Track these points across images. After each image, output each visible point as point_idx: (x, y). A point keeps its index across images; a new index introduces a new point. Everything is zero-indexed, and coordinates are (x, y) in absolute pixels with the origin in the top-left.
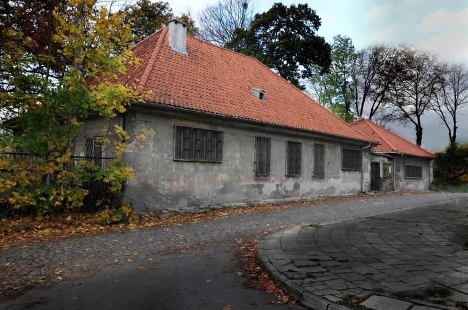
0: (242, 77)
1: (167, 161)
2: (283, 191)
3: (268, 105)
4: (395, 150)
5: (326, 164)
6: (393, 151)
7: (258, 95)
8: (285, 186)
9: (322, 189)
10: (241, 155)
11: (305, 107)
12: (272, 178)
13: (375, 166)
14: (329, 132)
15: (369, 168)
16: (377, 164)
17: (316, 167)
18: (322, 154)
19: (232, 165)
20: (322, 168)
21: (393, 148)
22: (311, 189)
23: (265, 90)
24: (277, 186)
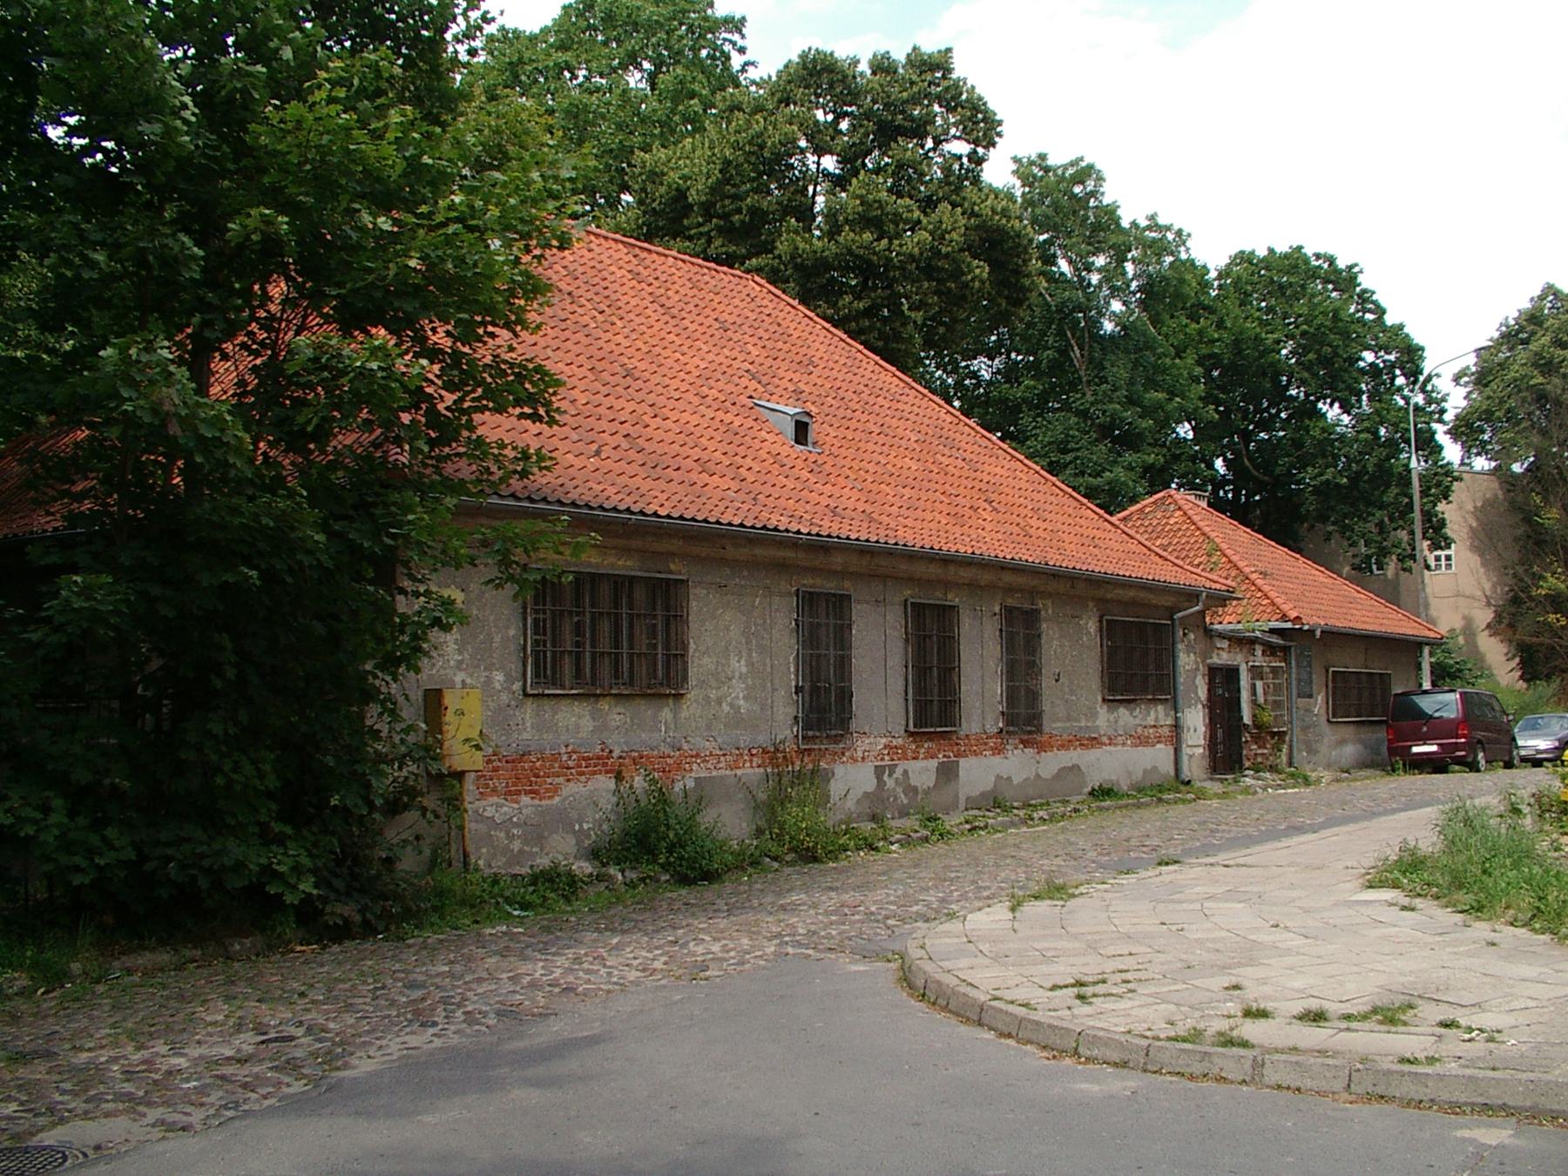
0: (721, 359)
1: (505, 697)
2: (899, 790)
3: (827, 468)
4: (1293, 614)
5: (1047, 682)
6: (1284, 618)
7: (790, 430)
8: (906, 772)
9: (1038, 776)
10: (750, 664)
11: (960, 463)
12: (862, 745)
13: (1223, 681)
14: (1054, 559)
15: (1202, 692)
16: (1231, 674)
17: (1012, 696)
18: (1032, 643)
19: (719, 702)
20: (1034, 697)
21: (1285, 607)
22: (998, 777)
23: (814, 410)
24: (879, 771)
